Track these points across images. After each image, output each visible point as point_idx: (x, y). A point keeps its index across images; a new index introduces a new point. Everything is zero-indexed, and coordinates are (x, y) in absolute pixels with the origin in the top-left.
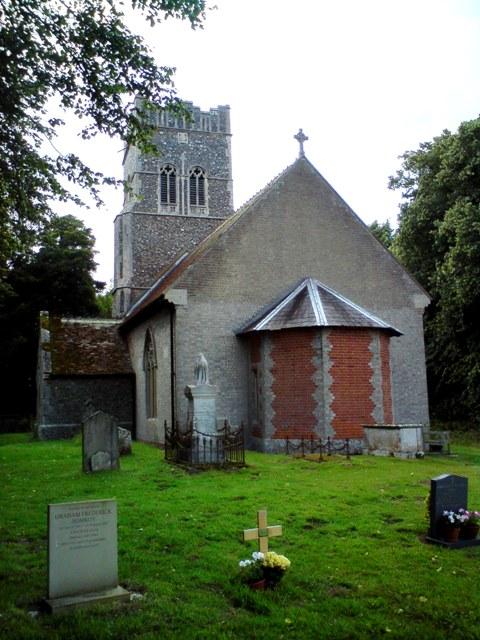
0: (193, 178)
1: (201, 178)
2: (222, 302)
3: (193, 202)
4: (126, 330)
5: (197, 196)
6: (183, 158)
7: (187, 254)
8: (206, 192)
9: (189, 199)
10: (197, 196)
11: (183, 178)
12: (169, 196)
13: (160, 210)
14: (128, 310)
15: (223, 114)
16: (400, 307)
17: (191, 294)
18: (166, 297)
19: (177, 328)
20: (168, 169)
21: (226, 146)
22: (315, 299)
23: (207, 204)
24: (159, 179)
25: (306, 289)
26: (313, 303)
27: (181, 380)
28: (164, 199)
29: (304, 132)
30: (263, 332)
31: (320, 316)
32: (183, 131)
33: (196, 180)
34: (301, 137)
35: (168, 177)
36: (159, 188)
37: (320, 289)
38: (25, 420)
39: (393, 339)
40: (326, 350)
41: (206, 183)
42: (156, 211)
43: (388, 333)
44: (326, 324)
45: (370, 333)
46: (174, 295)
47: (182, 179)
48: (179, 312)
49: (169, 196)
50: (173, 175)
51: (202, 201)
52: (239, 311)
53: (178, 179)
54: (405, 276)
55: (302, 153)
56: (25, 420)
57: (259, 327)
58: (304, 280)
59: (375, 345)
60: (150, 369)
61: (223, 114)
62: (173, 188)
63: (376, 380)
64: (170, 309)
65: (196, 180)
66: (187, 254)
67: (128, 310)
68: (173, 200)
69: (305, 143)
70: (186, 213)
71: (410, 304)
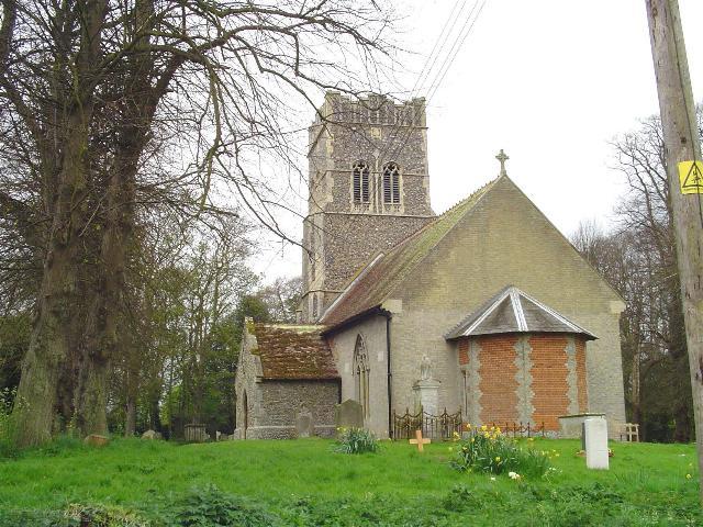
0: (387, 174)
1: (396, 174)
2: (433, 310)
3: (387, 200)
4: (330, 335)
5: (391, 194)
6: (376, 154)
7: (382, 255)
8: (401, 190)
9: (383, 197)
10: (391, 194)
11: (377, 175)
12: (362, 194)
13: (354, 210)
14: (322, 314)
15: (418, 106)
16: (597, 313)
17: (405, 301)
18: (383, 307)
19: (392, 327)
20: (361, 166)
21: (421, 140)
22: (518, 309)
23: (401, 202)
24: (352, 177)
25: (509, 297)
26: (515, 311)
27: (398, 380)
28: (357, 196)
29: (505, 152)
30: (472, 337)
31: (522, 323)
32: (375, 126)
33: (390, 172)
34: (502, 157)
35: (361, 171)
36: (352, 186)
37: (521, 297)
38: (630, 254)
39: (589, 342)
40: (527, 352)
41: (401, 180)
42: (348, 210)
43: (583, 338)
44: (527, 330)
45: (567, 338)
46: (393, 305)
47: (376, 177)
48: (394, 320)
49: (362, 194)
50: (366, 172)
51: (397, 199)
52: (448, 319)
53: (370, 177)
54: (602, 283)
55: (504, 173)
56: (630, 254)
57: (468, 332)
58: (506, 288)
59: (571, 348)
60: (362, 372)
61: (418, 106)
62: (366, 185)
63: (572, 379)
64: (387, 316)
65: (390, 172)
66: (382, 255)
67: (322, 314)
68: (366, 198)
69: (506, 162)
70: (380, 212)
71: (607, 310)
